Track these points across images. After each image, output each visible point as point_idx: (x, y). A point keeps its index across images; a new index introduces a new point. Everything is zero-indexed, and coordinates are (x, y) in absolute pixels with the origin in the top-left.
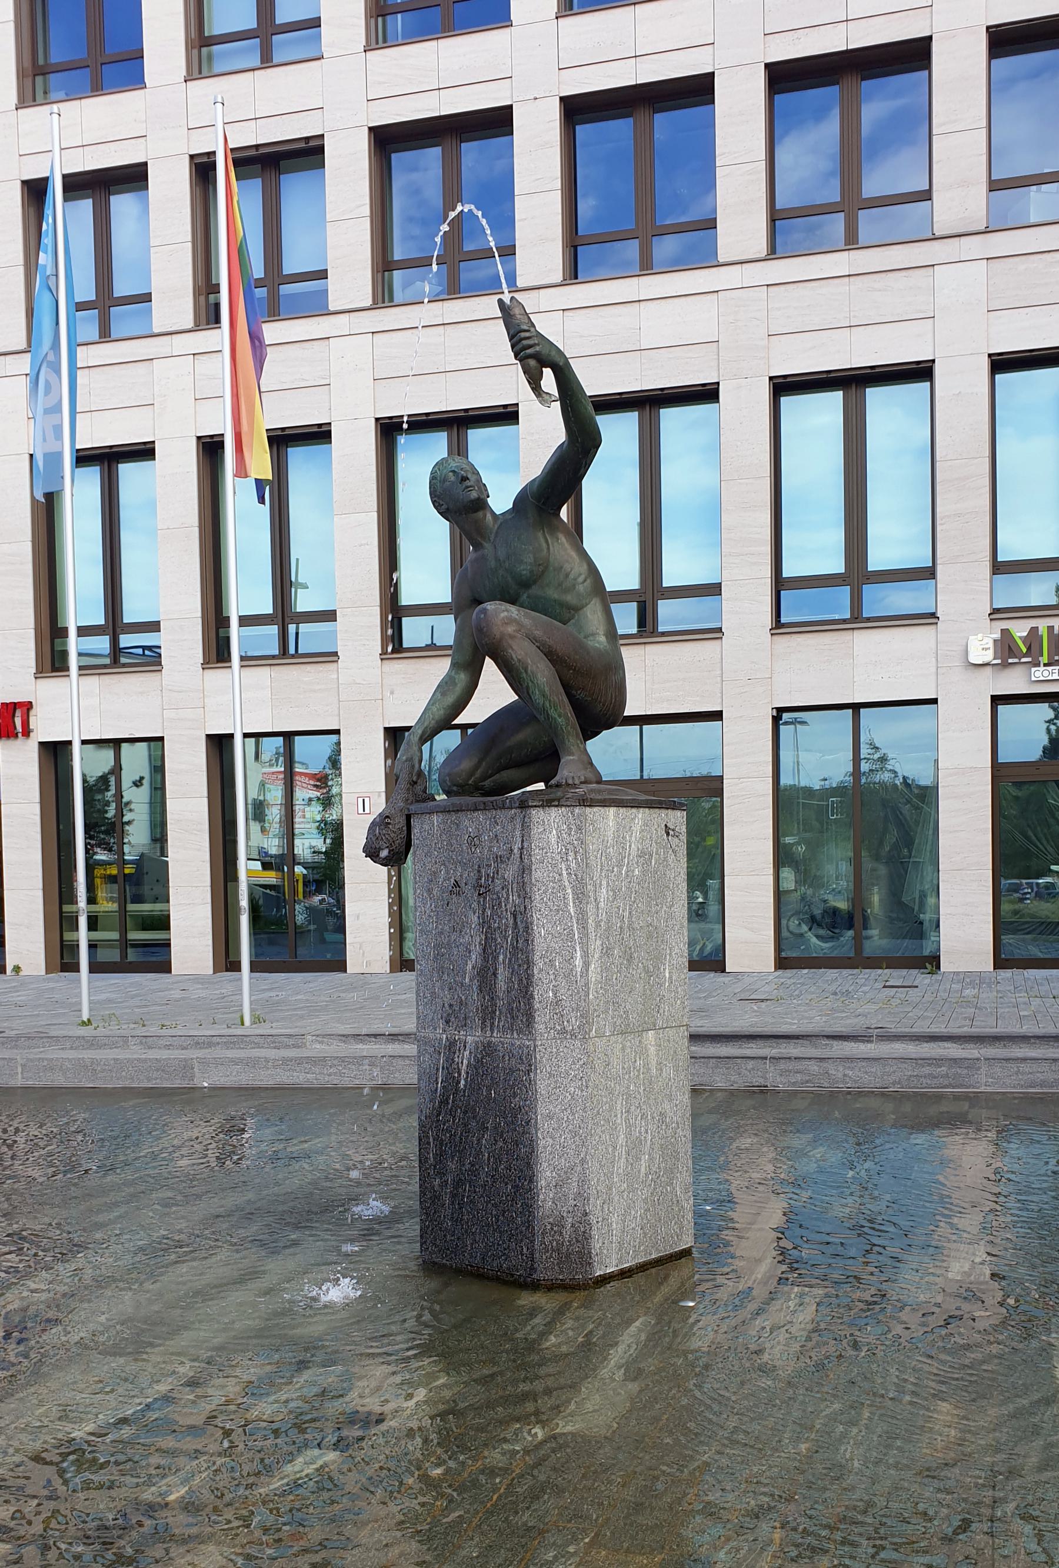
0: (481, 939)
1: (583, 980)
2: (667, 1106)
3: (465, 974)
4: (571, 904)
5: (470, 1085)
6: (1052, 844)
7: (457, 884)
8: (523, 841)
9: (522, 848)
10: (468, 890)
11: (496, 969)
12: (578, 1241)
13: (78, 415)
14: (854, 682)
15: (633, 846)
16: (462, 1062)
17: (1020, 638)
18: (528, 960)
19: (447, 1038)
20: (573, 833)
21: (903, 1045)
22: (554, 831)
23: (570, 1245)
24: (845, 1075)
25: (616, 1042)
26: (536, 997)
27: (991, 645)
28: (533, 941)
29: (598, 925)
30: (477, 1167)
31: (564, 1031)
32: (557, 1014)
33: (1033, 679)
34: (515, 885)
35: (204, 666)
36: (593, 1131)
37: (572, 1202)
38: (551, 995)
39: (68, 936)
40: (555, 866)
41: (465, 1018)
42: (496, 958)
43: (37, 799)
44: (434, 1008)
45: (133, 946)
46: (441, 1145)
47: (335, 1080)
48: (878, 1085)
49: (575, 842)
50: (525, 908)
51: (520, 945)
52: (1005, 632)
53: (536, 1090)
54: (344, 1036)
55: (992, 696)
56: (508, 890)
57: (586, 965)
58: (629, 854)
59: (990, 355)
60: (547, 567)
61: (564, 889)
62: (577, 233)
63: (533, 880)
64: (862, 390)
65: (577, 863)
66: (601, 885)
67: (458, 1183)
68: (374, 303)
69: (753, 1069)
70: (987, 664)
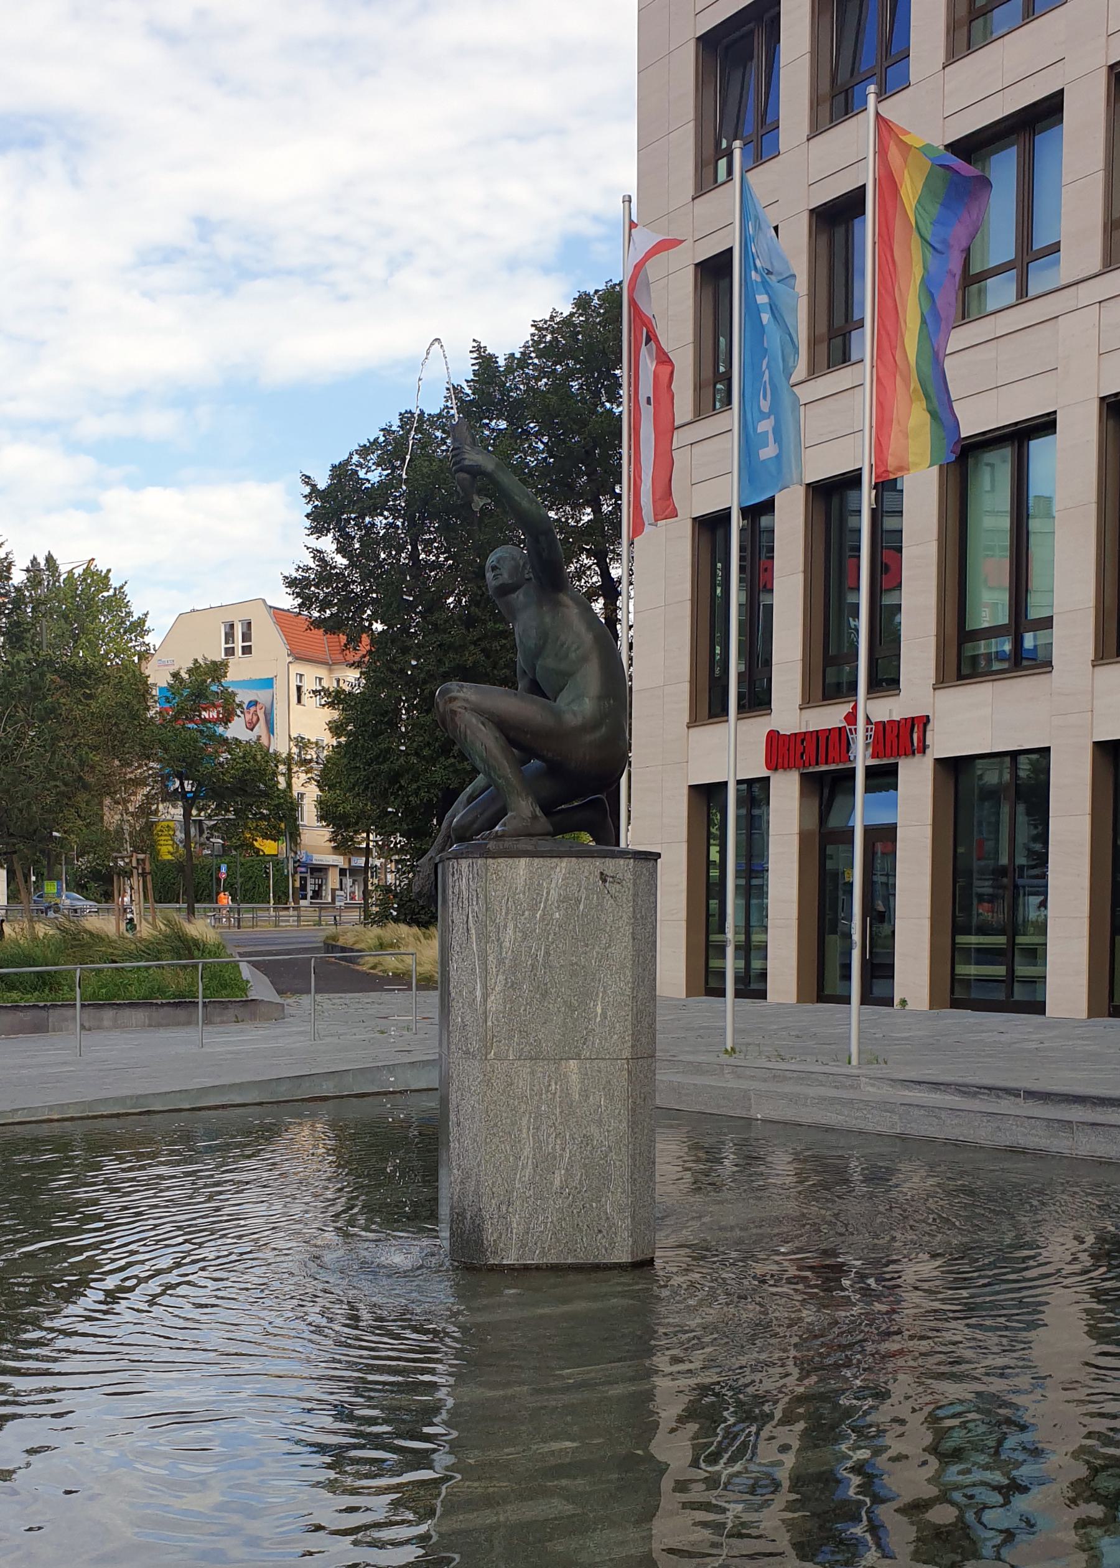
2: (594, 1130)
13: (954, 403)
15: (552, 891)
25: (524, 1066)
29: (501, 961)
31: (467, 1052)
35: (1095, 663)
36: (488, 1140)
39: (714, 963)
43: (930, 821)
45: (1018, 981)
47: (861, 1125)
54: (892, 1080)
57: (485, 996)
58: (547, 900)
65: (479, 908)
66: (505, 926)
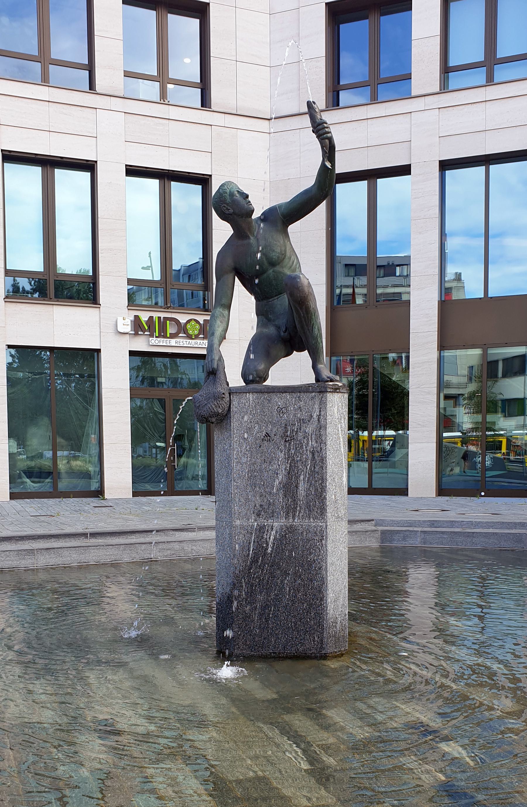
0: (286, 467)
3: (273, 487)
4: (342, 447)
5: (276, 550)
6: (157, 431)
7: (267, 435)
8: (320, 411)
9: (320, 415)
10: (277, 439)
11: (298, 483)
12: (342, 630)
14: (54, 335)
16: (270, 538)
17: (144, 321)
18: (322, 478)
19: (258, 524)
20: (343, 408)
21: (210, 532)
23: (340, 633)
24: (192, 549)
26: (328, 498)
27: (129, 323)
28: (326, 467)
30: (280, 596)
31: (338, 517)
33: (151, 344)
34: (313, 436)
37: (341, 609)
40: (336, 426)
41: (273, 513)
42: (298, 478)
44: (247, 508)
46: (252, 586)
48: (208, 554)
49: (344, 413)
50: (321, 448)
51: (317, 470)
52: (137, 317)
53: (327, 550)
55: (129, 351)
56: (308, 439)
59: (126, 165)
60: (285, 256)
63: (327, 433)
64: (53, 169)
67: (265, 607)
68: (327, 107)
69: (145, 549)
70: (127, 333)
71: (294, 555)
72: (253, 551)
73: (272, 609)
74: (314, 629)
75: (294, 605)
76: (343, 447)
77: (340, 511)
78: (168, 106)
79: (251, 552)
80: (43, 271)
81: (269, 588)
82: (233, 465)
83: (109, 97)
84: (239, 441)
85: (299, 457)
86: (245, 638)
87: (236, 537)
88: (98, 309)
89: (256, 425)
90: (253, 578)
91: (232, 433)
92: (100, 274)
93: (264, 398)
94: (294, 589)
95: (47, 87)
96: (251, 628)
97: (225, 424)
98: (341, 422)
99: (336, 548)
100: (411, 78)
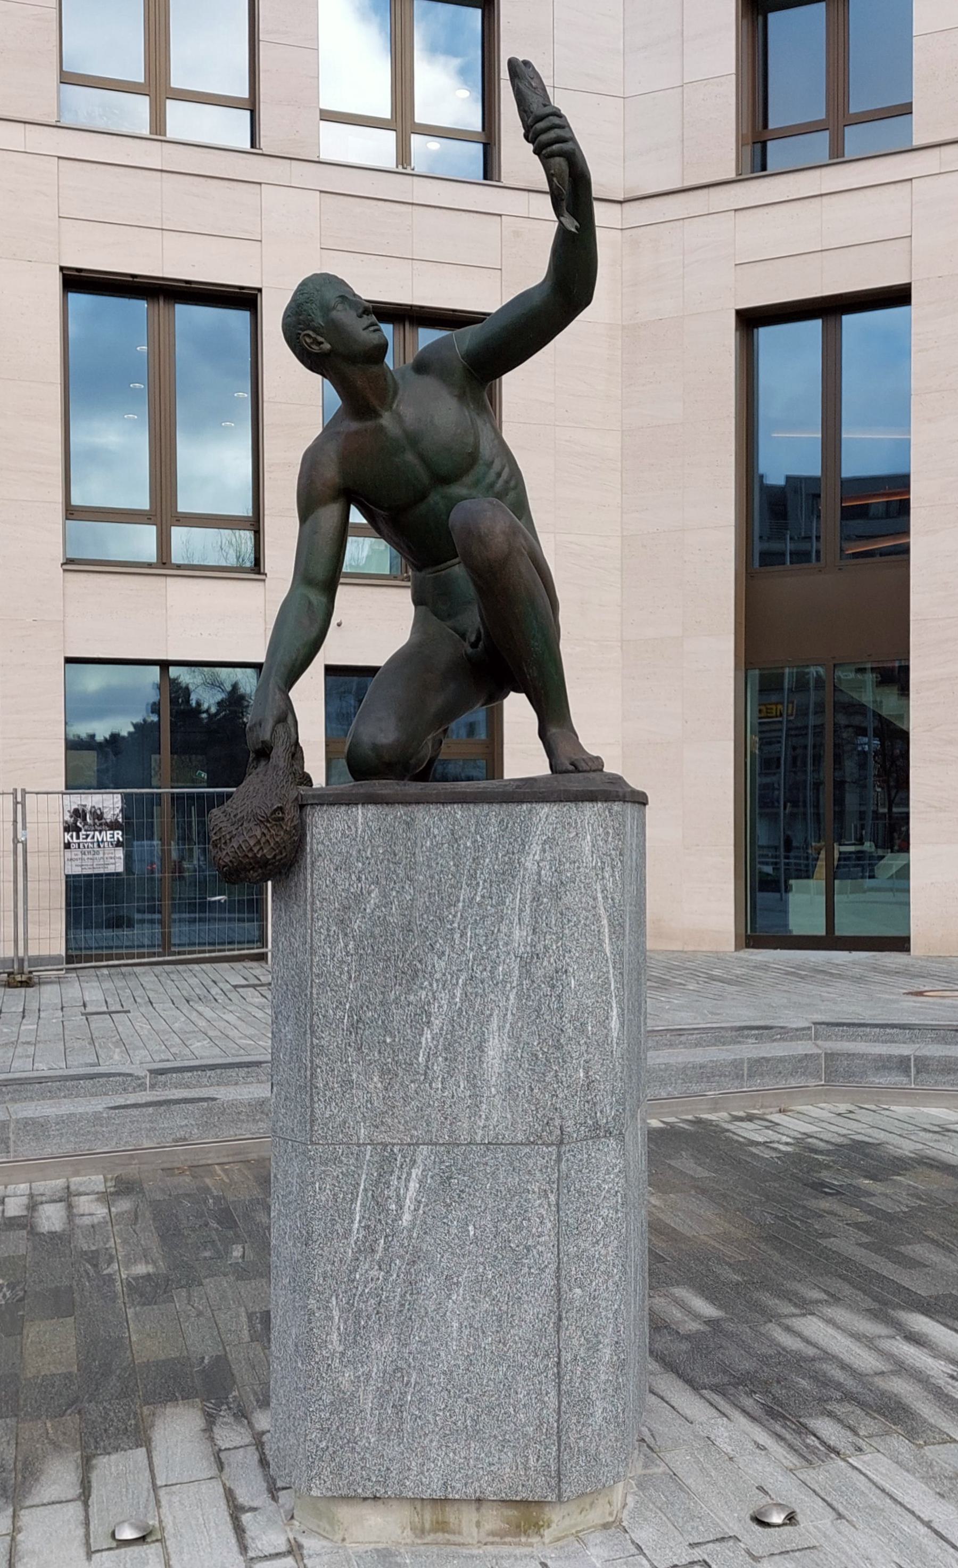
1: (619, 1049)
4: (607, 941)
20: (610, 839)
22: (589, 837)
30: (436, 1345)
31: (597, 1126)
32: (588, 1102)
38: (582, 1075)
40: (588, 886)
49: (613, 852)
61: (599, 920)
62: (765, 125)
65: (615, 882)
68: (738, 175)
71: (472, 1233)
72: (360, 1222)
73: (413, 1381)
74: (525, 1435)
75: (472, 1368)
76: (610, 939)
77: (601, 1112)
78: (410, 178)
79: (356, 1225)
80: (147, 507)
81: (403, 1324)
82: (311, 993)
83: (289, 161)
84: (328, 930)
85: (489, 969)
86: (337, 1460)
87: (317, 1186)
88: (261, 584)
89: (373, 887)
90: (361, 1295)
91: (309, 907)
92: (266, 513)
93: (395, 817)
94: (471, 1326)
95: (159, 144)
96: (353, 1431)
97: (293, 884)
98: (603, 878)
99: (591, 1211)
100: (911, 113)
